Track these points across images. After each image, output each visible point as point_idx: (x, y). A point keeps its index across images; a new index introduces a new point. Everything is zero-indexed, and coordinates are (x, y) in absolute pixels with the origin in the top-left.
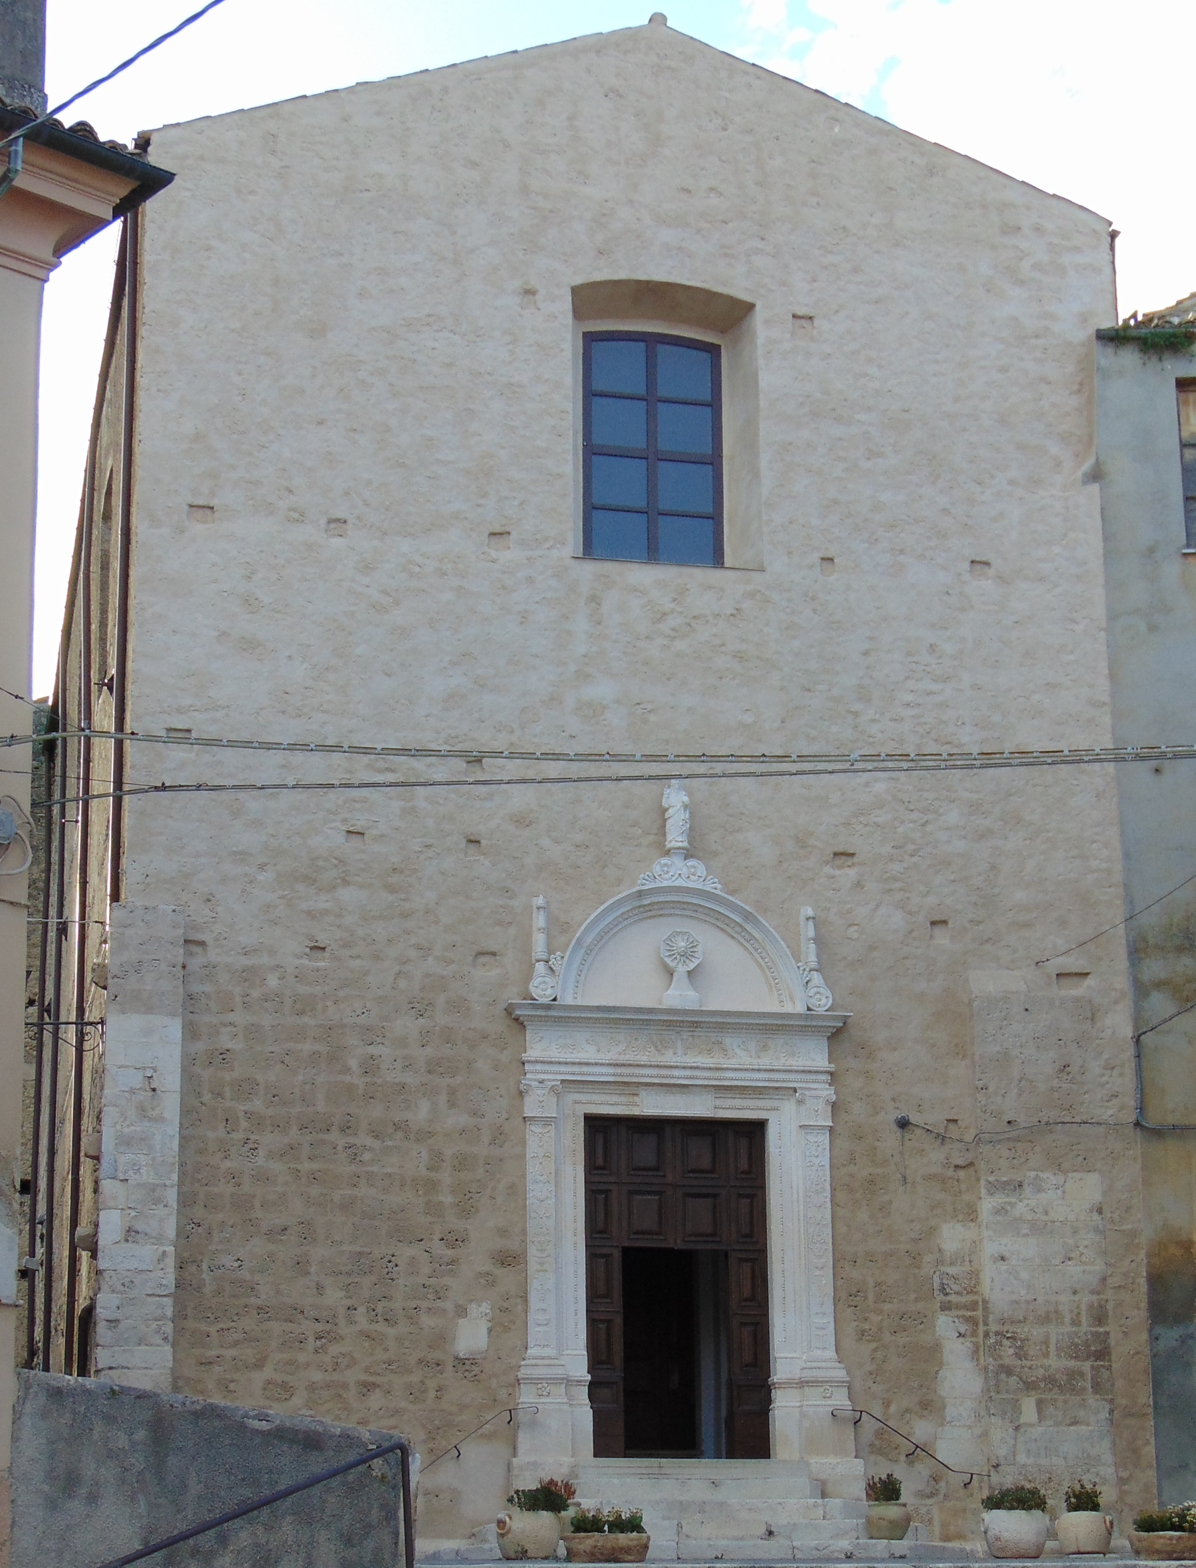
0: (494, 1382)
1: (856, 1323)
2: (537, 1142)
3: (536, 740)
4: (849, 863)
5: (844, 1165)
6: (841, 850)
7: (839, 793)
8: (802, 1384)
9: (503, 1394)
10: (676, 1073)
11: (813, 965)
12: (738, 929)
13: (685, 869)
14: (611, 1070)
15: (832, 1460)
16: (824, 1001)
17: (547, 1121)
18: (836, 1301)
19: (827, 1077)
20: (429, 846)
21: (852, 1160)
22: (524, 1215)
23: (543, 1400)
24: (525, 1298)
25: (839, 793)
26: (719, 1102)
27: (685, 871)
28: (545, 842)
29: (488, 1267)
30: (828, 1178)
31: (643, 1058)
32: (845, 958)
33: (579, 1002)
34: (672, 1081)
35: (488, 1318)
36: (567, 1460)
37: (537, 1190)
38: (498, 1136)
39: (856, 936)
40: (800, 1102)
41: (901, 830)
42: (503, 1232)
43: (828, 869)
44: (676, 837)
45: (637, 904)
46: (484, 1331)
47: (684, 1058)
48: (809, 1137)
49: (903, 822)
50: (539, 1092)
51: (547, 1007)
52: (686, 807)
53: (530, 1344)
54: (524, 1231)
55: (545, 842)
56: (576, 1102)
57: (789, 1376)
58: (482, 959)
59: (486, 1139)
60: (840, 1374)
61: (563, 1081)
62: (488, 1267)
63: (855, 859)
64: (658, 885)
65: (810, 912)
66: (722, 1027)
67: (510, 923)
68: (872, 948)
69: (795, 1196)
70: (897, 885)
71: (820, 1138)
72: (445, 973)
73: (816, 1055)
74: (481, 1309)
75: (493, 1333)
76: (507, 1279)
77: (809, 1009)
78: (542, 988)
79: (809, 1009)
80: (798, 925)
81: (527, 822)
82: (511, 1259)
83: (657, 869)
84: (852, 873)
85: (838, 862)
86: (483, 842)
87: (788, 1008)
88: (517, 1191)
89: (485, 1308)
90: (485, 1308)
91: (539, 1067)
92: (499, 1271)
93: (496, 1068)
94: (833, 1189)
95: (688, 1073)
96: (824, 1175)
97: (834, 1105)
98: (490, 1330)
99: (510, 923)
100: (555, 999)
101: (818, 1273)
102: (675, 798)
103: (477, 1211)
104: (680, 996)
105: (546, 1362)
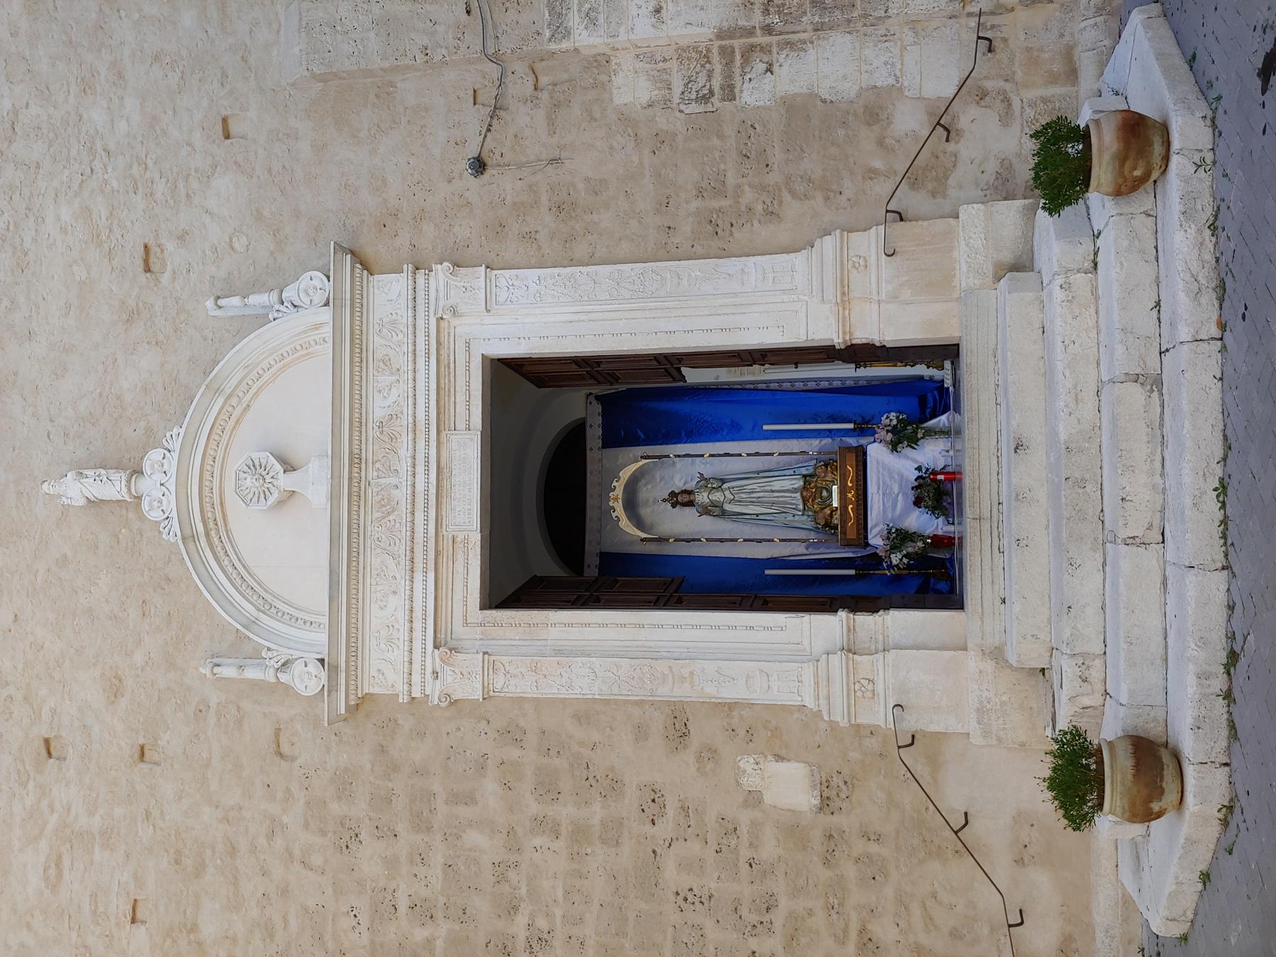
0: (854, 755)
1: (756, 223)
2: (518, 681)
3: (20, 667)
4: (158, 250)
5: (539, 248)
6: (139, 263)
7: (75, 268)
8: (844, 297)
9: (872, 743)
10: (420, 487)
11: (274, 296)
12: (234, 401)
13: (154, 477)
14: (419, 577)
15: (961, 252)
16: (316, 283)
17: (490, 666)
18: (724, 254)
19: (421, 276)
20: (148, 814)
21: (530, 237)
22: (616, 702)
23: (880, 688)
24: (731, 706)
25: (75, 268)
26: (461, 425)
27: (159, 477)
28: (139, 658)
29: (689, 756)
30: (556, 270)
31: (404, 534)
32: (272, 253)
33: (325, 620)
34: (433, 490)
35: (761, 760)
36: (972, 662)
37: (582, 681)
38: (512, 735)
39: (244, 240)
40: (454, 312)
41: (115, 184)
42: (641, 733)
43: (165, 279)
44: (113, 488)
45: (203, 540)
46: (782, 766)
47: (399, 476)
48: (501, 299)
49: (106, 182)
50: (450, 679)
51: (333, 670)
53: (794, 700)
54: (639, 703)
55: (139, 658)
56: (466, 624)
57: (833, 321)
58: (285, 749)
59: (514, 753)
60: (828, 244)
61: (436, 647)
62: (689, 756)
63: (151, 243)
64: (174, 514)
65: (210, 303)
66: (358, 424)
67: (239, 708)
68: (259, 216)
69: (582, 317)
70: (181, 184)
71: (502, 283)
72: (302, 802)
73: (388, 292)
74: (749, 770)
75: (783, 753)
76: (704, 731)
77: (327, 304)
78: (307, 680)
79: (327, 304)
80: (232, 317)
81: (117, 682)
82: (678, 724)
83: (156, 515)
84: (170, 246)
85: (155, 267)
86: (141, 741)
87: (327, 331)
88: (586, 712)
89: (747, 763)
90: (747, 763)
91: (416, 678)
92: (695, 741)
93: (422, 735)
94: (572, 263)
95: (420, 469)
96: (553, 277)
97: (457, 265)
98: (779, 758)
99: (239, 708)
100: (322, 661)
101: (685, 282)
102: (75, 490)
103: (612, 769)
104: (314, 484)
105: (823, 684)
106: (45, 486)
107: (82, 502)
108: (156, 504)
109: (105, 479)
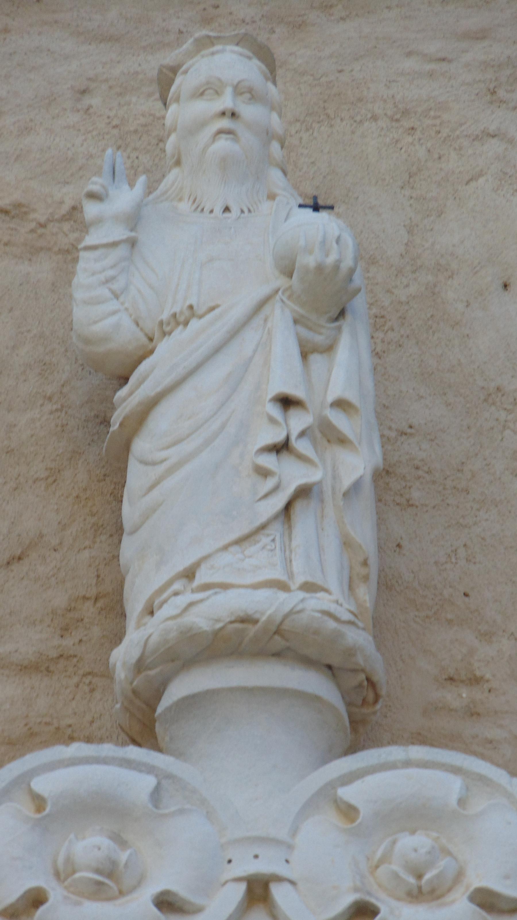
44: (213, 534)
52: (325, 302)
106: (230, 64)
107: (101, 306)
108: (90, 846)
109: (293, 475)
